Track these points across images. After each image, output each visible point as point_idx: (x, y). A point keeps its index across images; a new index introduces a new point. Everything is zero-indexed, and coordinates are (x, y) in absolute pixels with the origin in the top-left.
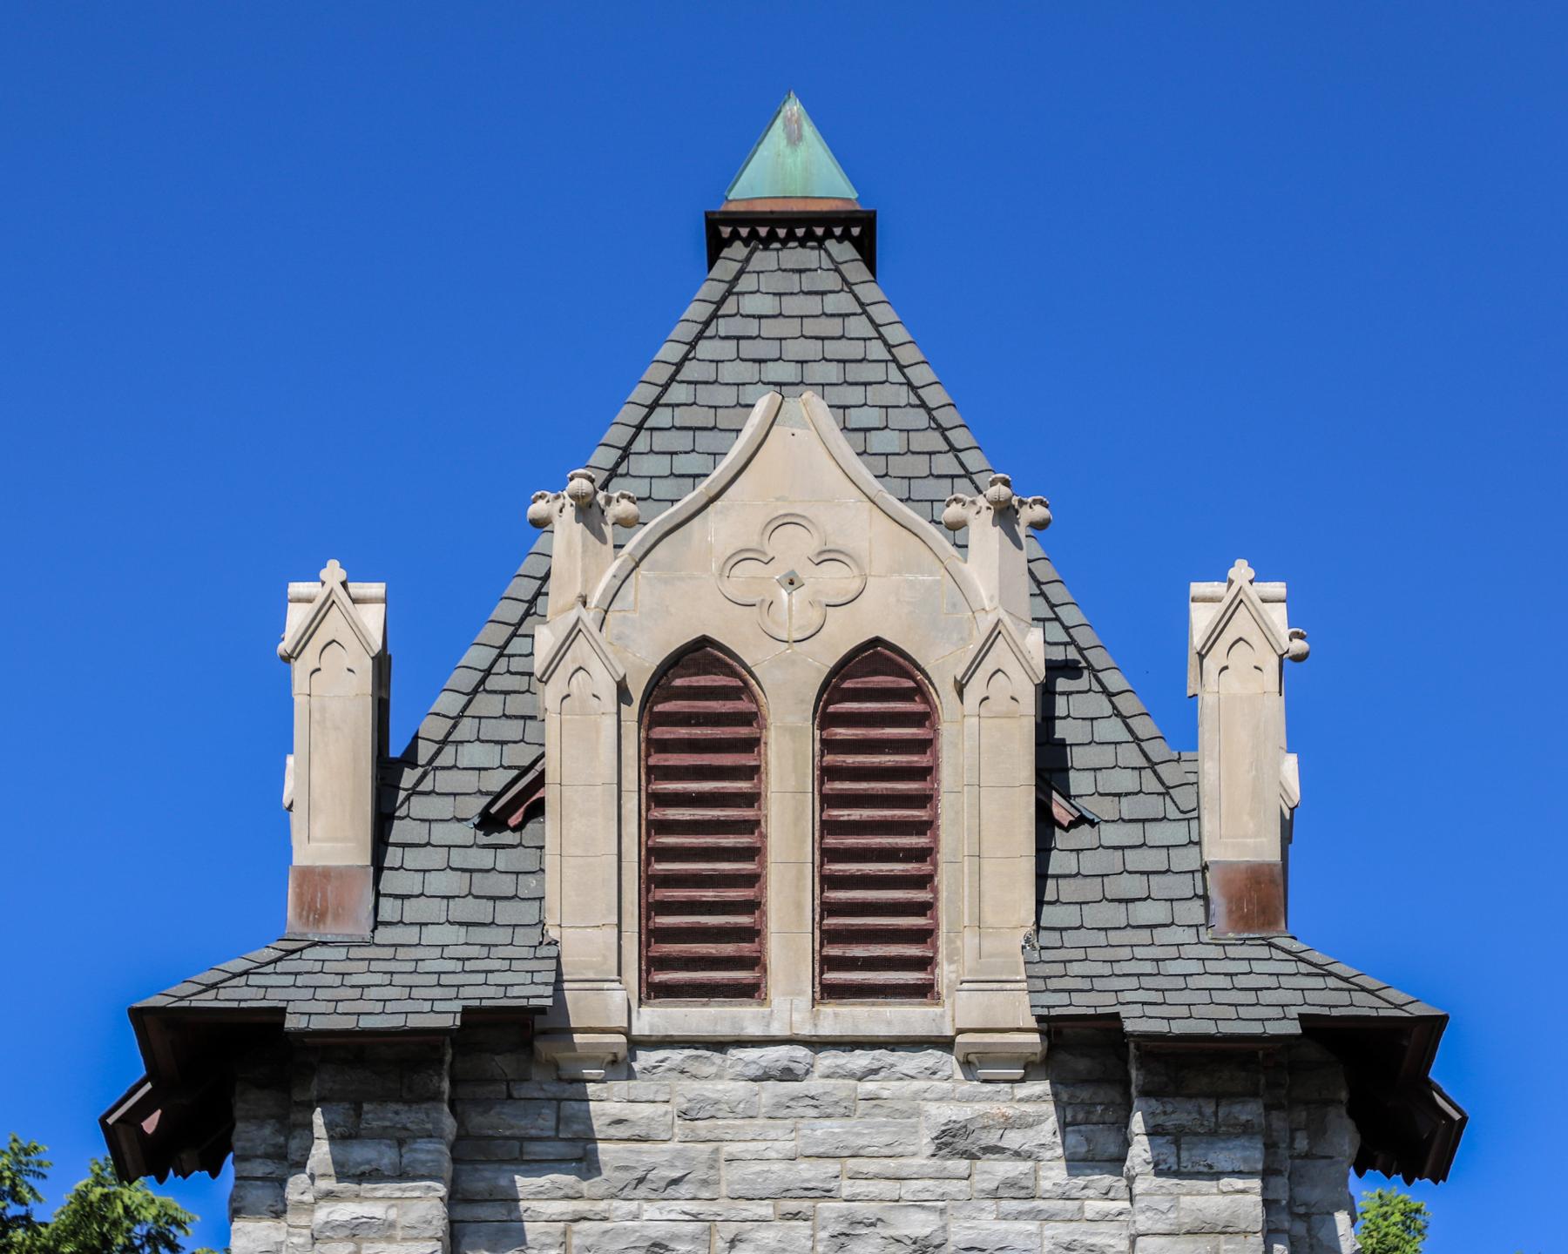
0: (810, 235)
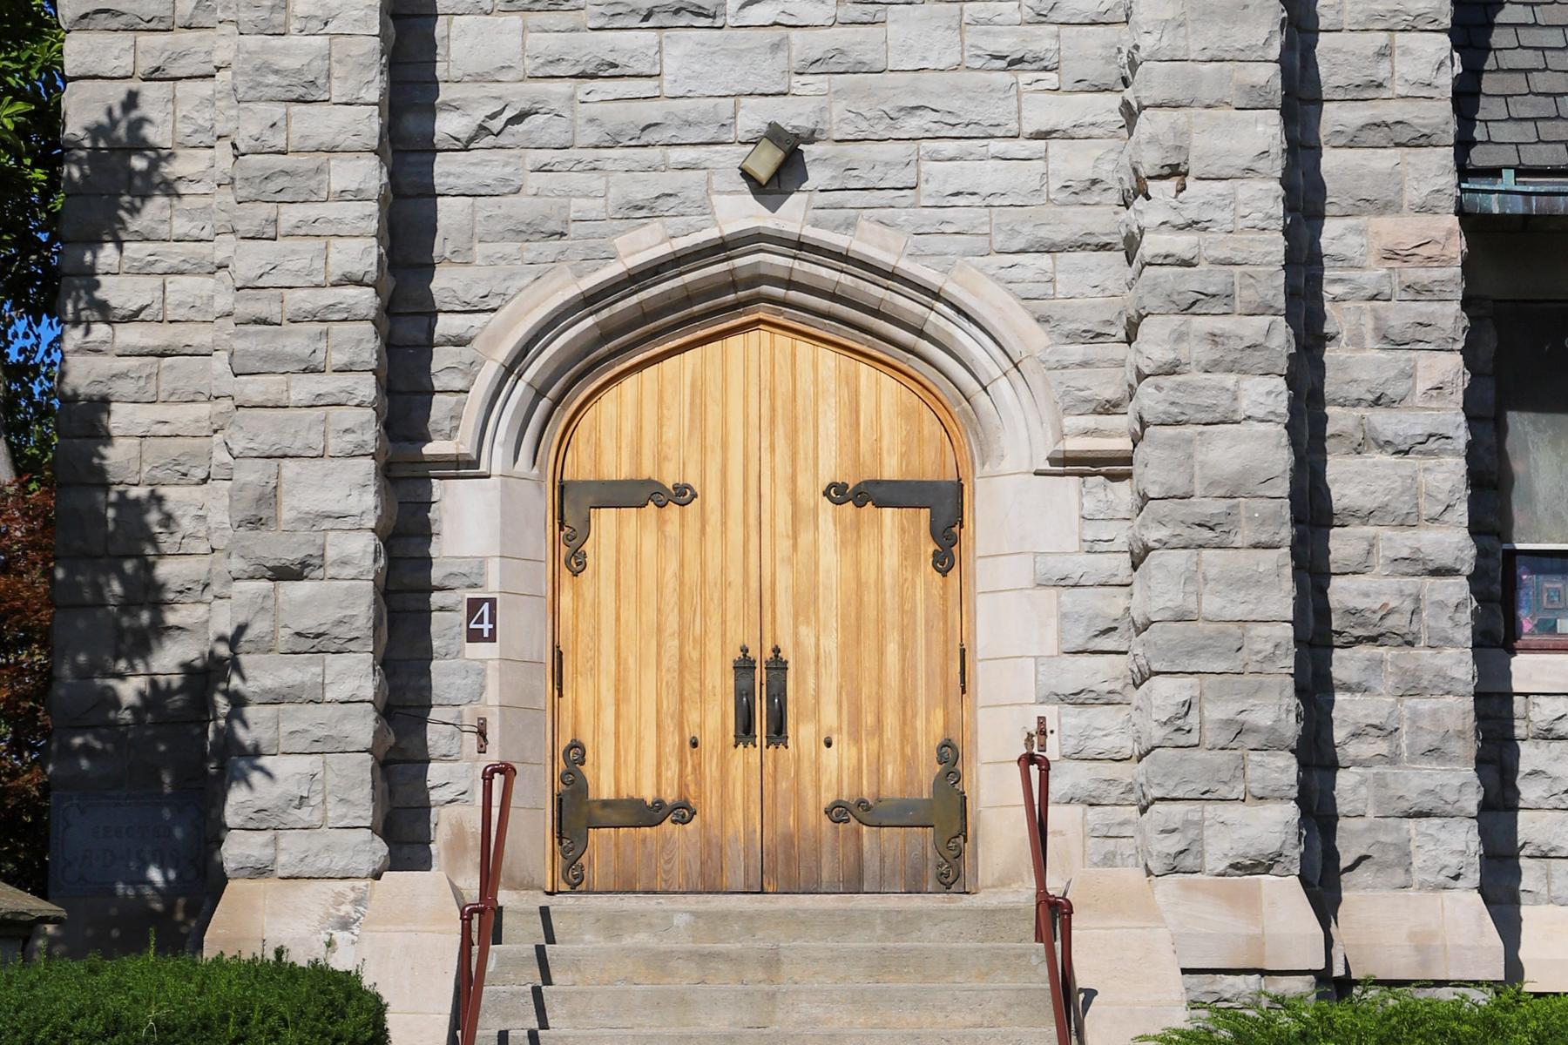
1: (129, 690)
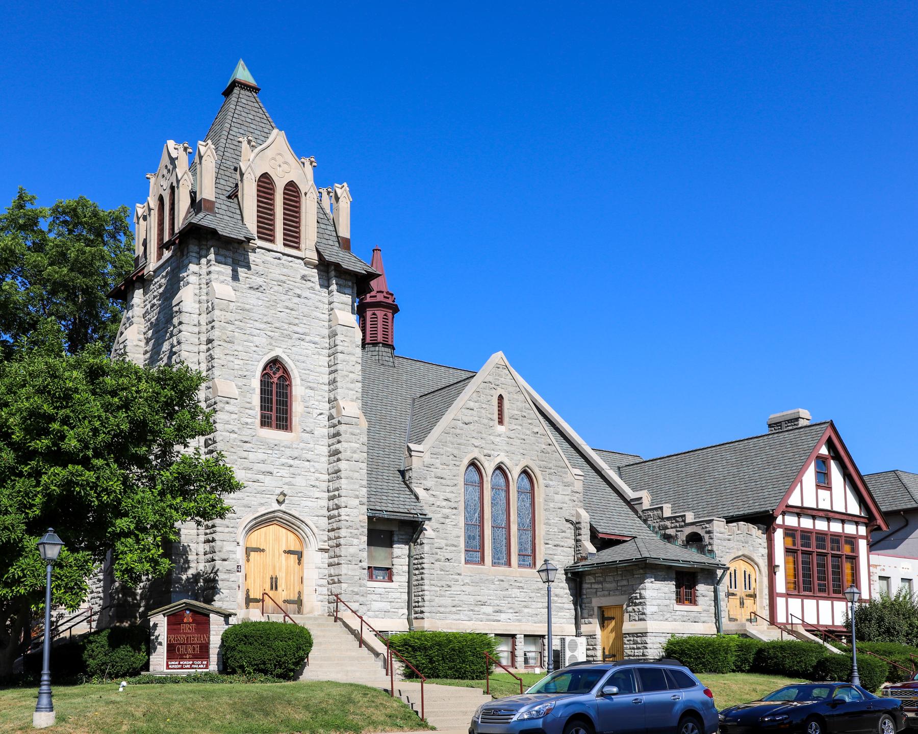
1: (184, 577)
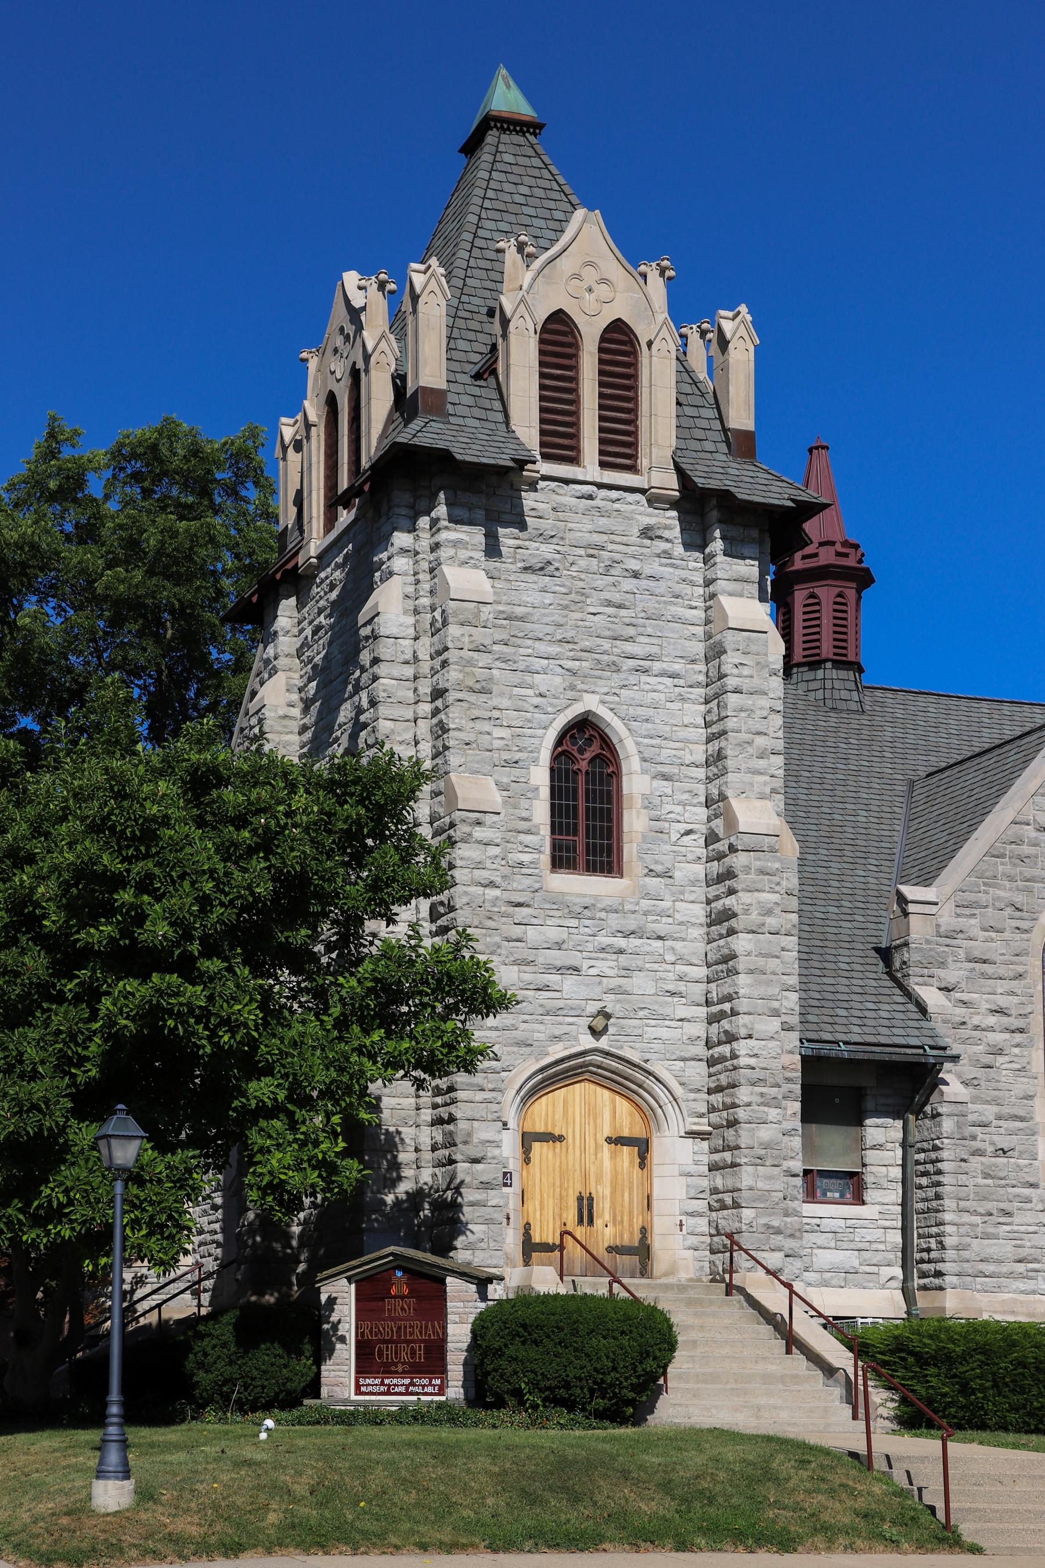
0: (521, 131)
1: (390, 1199)
